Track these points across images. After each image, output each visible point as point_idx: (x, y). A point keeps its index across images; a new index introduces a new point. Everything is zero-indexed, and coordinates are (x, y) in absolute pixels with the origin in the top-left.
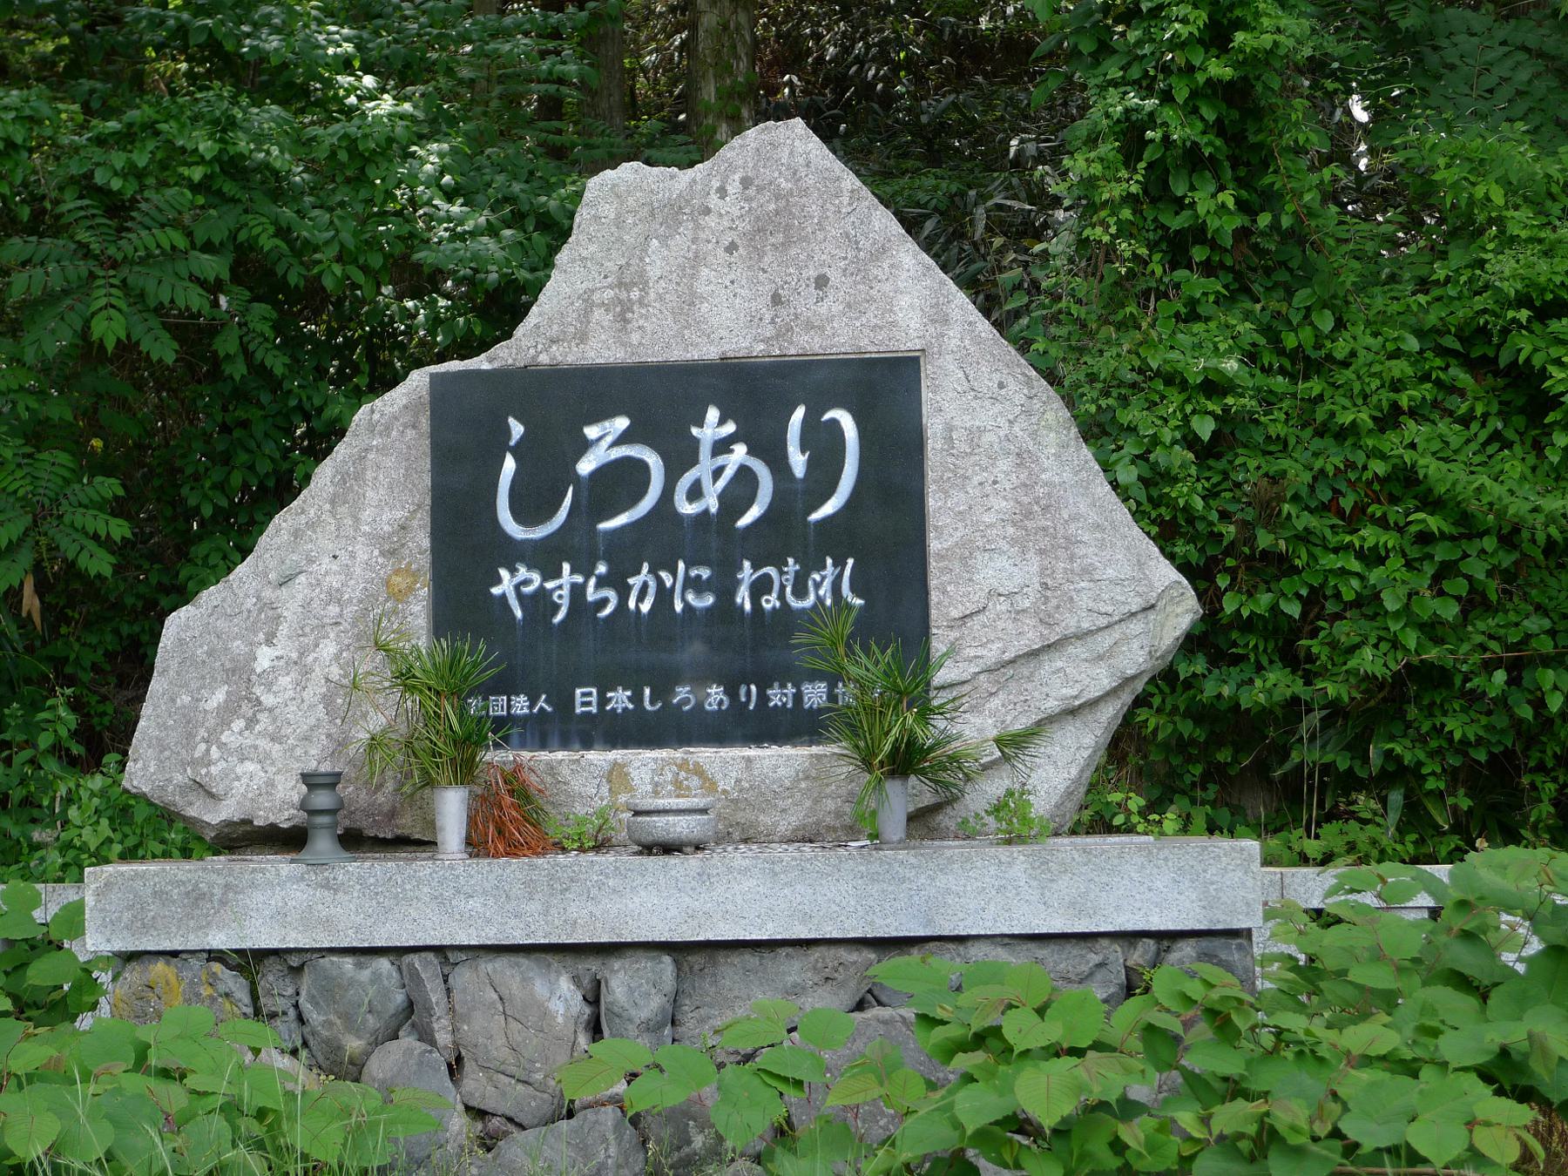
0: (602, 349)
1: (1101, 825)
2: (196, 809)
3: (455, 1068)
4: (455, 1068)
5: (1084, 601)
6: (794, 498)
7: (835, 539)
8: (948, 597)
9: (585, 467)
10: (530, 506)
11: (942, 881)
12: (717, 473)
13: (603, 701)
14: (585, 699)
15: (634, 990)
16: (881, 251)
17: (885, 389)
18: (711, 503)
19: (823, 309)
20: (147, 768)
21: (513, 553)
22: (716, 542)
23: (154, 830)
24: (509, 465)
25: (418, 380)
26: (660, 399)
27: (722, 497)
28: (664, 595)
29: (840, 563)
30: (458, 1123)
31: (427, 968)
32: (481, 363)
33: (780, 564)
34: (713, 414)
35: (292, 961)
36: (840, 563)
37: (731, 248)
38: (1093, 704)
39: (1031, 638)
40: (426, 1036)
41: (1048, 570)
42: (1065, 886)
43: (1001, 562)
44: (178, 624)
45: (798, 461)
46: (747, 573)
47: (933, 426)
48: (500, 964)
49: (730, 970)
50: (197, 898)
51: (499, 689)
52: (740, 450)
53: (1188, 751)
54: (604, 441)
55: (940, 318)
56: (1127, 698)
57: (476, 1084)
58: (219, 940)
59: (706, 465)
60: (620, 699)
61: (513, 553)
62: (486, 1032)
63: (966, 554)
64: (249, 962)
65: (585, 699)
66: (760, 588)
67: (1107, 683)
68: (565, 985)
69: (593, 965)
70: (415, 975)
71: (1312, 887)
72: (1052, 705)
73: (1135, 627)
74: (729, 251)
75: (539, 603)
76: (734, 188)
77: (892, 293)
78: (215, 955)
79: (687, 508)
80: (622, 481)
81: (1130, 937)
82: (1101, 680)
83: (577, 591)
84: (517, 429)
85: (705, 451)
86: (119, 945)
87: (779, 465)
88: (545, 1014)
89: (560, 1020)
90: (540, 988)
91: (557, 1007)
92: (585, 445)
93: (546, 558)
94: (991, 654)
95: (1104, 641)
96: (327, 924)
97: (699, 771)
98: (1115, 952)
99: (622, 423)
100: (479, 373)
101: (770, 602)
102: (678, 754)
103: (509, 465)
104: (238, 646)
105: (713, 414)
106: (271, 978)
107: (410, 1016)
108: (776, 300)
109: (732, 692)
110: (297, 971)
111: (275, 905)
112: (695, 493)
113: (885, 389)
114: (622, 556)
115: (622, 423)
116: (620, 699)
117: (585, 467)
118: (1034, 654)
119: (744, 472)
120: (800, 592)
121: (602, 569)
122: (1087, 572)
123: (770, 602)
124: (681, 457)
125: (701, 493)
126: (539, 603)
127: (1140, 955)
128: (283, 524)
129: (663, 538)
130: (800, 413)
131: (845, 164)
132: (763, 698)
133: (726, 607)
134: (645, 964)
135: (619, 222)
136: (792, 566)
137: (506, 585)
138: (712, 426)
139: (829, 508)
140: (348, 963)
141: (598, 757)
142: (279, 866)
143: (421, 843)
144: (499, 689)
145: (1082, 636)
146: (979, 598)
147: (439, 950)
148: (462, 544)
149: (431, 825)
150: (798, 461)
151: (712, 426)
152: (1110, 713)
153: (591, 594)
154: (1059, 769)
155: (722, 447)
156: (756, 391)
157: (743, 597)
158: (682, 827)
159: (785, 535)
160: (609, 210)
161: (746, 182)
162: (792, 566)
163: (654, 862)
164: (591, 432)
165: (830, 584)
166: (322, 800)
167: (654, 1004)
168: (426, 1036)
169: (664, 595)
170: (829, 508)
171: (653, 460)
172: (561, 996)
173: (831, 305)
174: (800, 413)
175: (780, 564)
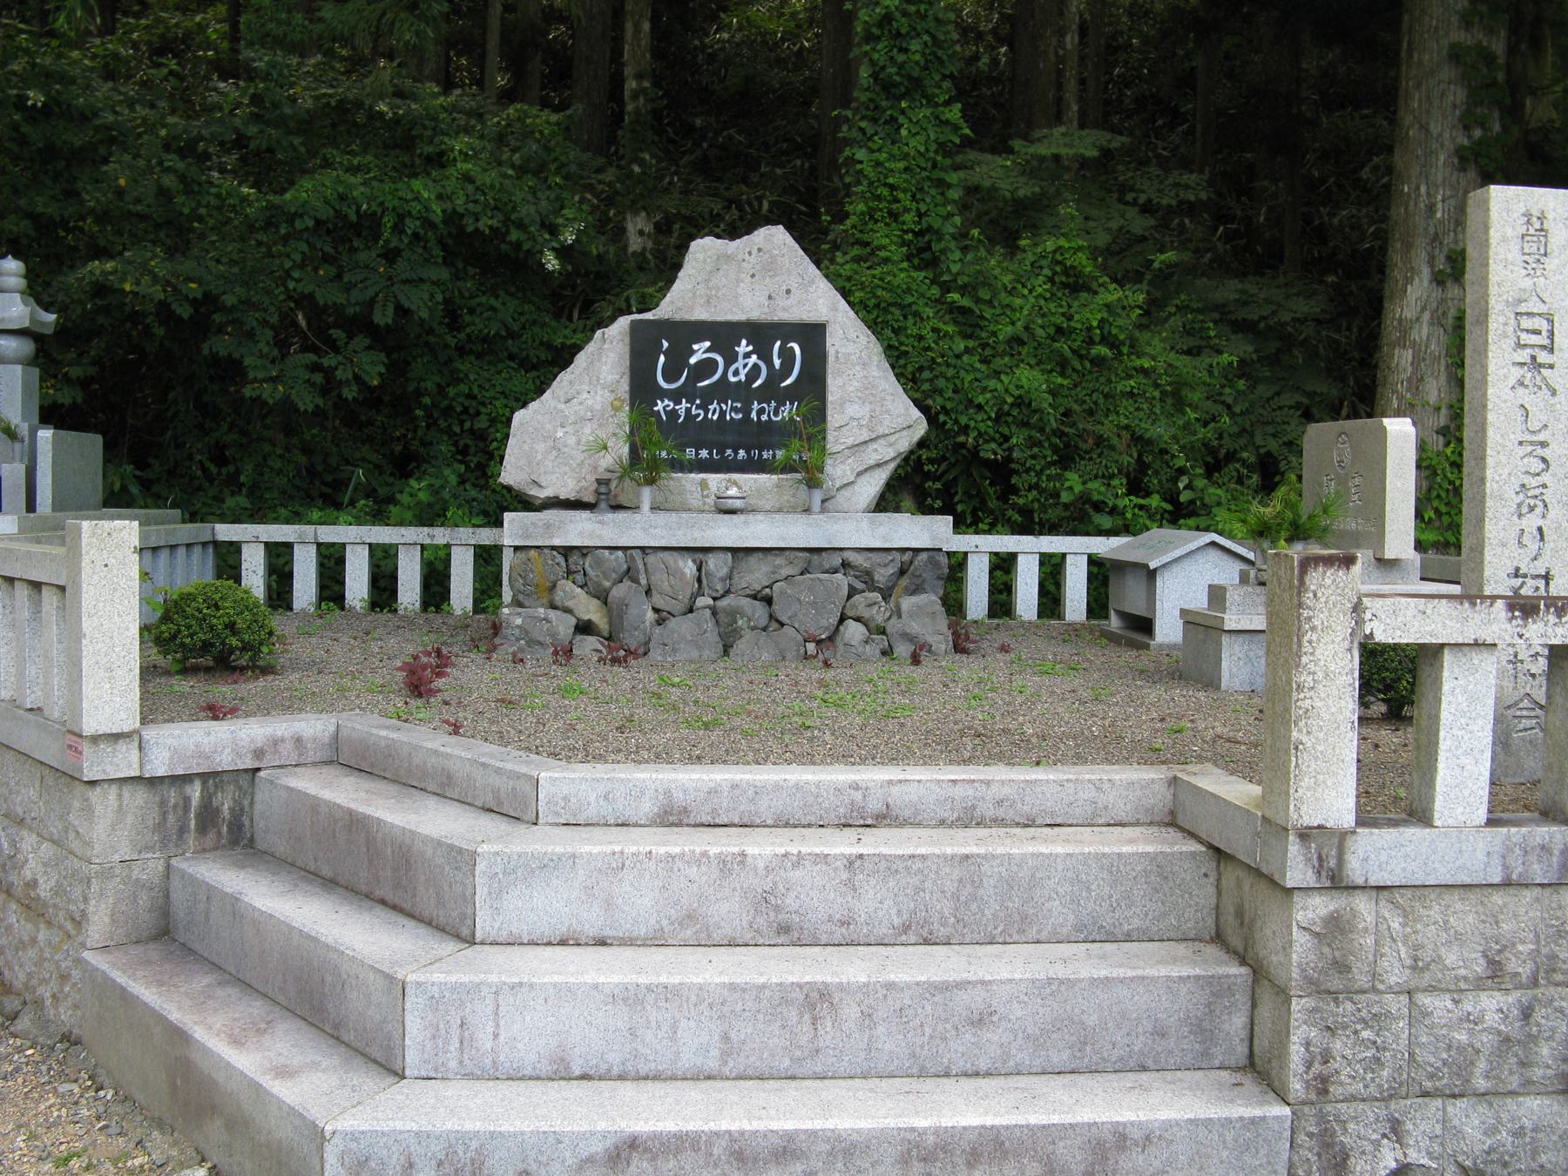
0: (701, 314)
2: (534, 492)
3: (648, 592)
4: (648, 592)
5: (886, 423)
6: (775, 377)
7: (791, 394)
8: (834, 418)
9: (693, 361)
11: (836, 527)
12: (745, 366)
13: (697, 454)
15: (717, 566)
16: (812, 282)
17: (812, 335)
19: (789, 303)
20: (511, 473)
21: (663, 394)
22: (743, 392)
23: (524, 503)
24: (662, 358)
25: (624, 322)
26: (724, 335)
28: (723, 413)
29: (792, 404)
30: (650, 616)
31: (637, 554)
32: (648, 316)
33: (769, 404)
34: (744, 342)
35: (583, 551)
36: (792, 404)
37: (753, 276)
39: (865, 436)
40: (636, 581)
41: (871, 409)
42: (882, 530)
43: (856, 406)
44: (519, 417)
45: (777, 362)
46: (756, 406)
47: (831, 351)
48: (666, 555)
49: (753, 560)
50: (548, 526)
51: (660, 445)
52: (754, 357)
53: (910, 486)
54: (700, 351)
55: (835, 309)
58: (557, 542)
59: (741, 362)
60: (704, 453)
61: (663, 394)
62: (661, 580)
64: (566, 551)
66: (761, 412)
67: (892, 455)
68: (690, 563)
69: (700, 556)
70: (632, 557)
72: (872, 462)
73: (904, 433)
75: (673, 414)
76: (755, 251)
77: (812, 296)
78: (553, 548)
79: (733, 379)
80: (707, 367)
81: (903, 550)
83: (688, 410)
84: (666, 344)
86: (517, 543)
87: (770, 364)
88: (683, 574)
90: (681, 563)
91: (687, 571)
92: (693, 352)
93: (676, 396)
94: (850, 441)
95: (892, 439)
96: (599, 537)
97: (735, 483)
98: (897, 555)
99: (708, 344)
101: (764, 418)
102: (727, 476)
103: (662, 358)
105: (744, 342)
106: (574, 558)
107: (629, 574)
108: (770, 297)
109: (748, 452)
110: (584, 555)
111: (578, 529)
112: (736, 373)
113: (812, 335)
114: (707, 396)
115: (708, 344)
116: (704, 453)
117: (693, 361)
119: (755, 366)
120: (776, 414)
122: (888, 412)
123: (764, 418)
124: (731, 358)
125: (739, 373)
126: (673, 414)
127: (907, 557)
128: (564, 377)
129: (723, 390)
130: (778, 343)
131: (1494, 743)
132: (760, 455)
134: (721, 555)
135: (705, 261)
136: (773, 404)
137: (660, 407)
138: (743, 347)
139: (788, 382)
140: (607, 552)
142: (585, 514)
143: (636, 508)
144: (660, 445)
146: (846, 419)
147: (642, 549)
148: (642, 389)
150: (777, 362)
151: (743, 347)
152: (892, 466)
153: (694, 412)
154: (873, 486)
156: (761, 334)
157: (754, 415)
158: (738, 504)
159: (771, 391)
160: (701, 256)
161: (759, 250)
164: (695, 347)
166: (603, 489)
167: (724, 571)
168: (636, 581)
169: (723, 413)
170: (788, 382)
171: (720, 359)
172: (688, 567)
173: (793, 300)
174: (778, 343)
175: (769, 404)
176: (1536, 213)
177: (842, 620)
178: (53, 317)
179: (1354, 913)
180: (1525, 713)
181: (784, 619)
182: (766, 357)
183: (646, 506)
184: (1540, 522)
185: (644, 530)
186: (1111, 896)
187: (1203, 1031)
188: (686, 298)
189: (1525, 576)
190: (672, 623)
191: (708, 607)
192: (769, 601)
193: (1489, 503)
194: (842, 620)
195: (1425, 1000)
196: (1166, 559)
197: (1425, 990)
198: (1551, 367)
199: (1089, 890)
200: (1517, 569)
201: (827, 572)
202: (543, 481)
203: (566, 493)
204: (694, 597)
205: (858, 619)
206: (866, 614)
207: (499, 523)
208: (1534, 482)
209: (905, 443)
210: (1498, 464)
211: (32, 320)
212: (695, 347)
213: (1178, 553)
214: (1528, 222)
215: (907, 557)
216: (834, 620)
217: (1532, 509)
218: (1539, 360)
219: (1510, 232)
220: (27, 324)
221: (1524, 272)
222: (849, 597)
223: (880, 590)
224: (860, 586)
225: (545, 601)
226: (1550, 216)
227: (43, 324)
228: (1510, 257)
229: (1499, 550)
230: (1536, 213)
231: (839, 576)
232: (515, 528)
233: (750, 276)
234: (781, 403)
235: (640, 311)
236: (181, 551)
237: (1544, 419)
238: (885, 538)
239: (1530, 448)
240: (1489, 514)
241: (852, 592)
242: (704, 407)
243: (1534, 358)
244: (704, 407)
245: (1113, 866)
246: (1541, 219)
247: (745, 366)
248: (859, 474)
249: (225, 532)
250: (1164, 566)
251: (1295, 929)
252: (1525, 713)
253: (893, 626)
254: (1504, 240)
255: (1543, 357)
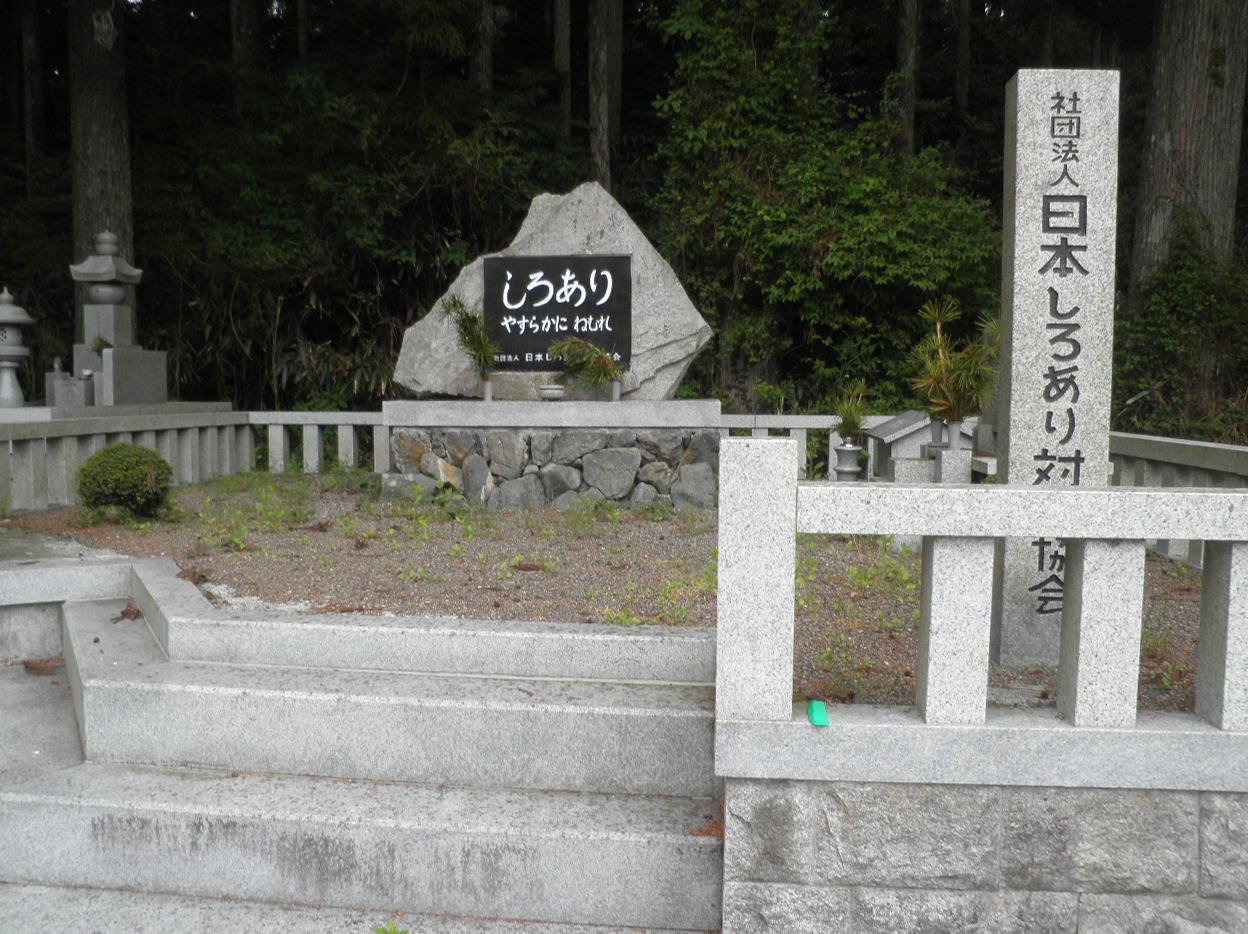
0: (536, 251)
1: (676, 397)
3: (489, 463)
4: (489, 463)
6: (593, 297)
8: (637, 328)
10: (513, 299)
12: (569, 290)
14: (528, 357)
17: (620, 265)
18: (567, 299)
20: (399, 377)
22: (568, 310)
23: (403, 393)
25: (480, 260)
26: (553, 267)
27: (571, 298)
28: (553, 326)
32: (499, 255)
33: (587, 317)
34: (568, 272)
36: (605, 317)
38: (680, 361)
39: (662, 340)
40: (480, 453)
41: (667, 317)
44: (409, 332)
45: (594, 287)
46: (578, 321)
54: (536, 280)
56: (690, 360)
57: (495, 467)
62: (498, 453)
63: (641, 318)
65: (528, 357)
66: (581, 324)
67: (684, 355)
71: (910, 140)
74: (578, 221)
75: (515, 328)
77: (628, 238)
80: (541, 291)
82: (681, 354)
83: (527, 325)
85: (566, 283)
87: (588, 288)
89: (107, 236)
92: (530, 281)
93: (517, 314)
95: (683, 343)
100: (498, 259)
101: (584, 329)
104: (427, 340)
112: (563, 295)
113: (620, 265)
116: (539, 357)
118: (661, 346)
120: (593, 325)
121: (534, 318)
123: (584, 329)
124: (558, 284)
125: (564, 294)
129: (553, 309)
130: (594, 273)
133: (571, 330)
136: (591, 318)
137: (506, 322)
138: (568, 276)
141: (532, 374)
144: (491, 346)
145: (676, 341)
149: (483, 393)
150: (594, 287)
151: (568, 276)
152: (684, 364)
153: (531, 326)
154: (669, 380)
155: (571, 282)
156: (581, 266)
157: (576, 327)
159: (591, 308)
161: (580, 201)
162: (573, 276)
163: (546, 404)
164: (532, 277)
165: (603, 323)
168: (480, 453)
169: (553, 326)
174: (594, 273)
175: (587, 317)
176: (1067, 95)
177: (637, 481)
178: (138, 272)
179: (790, 806)
180: (1052, 594)
181: (590, 482)
182: (586, 283)
183: (488, 396)
184: (1070, 405)
185: (484, 413)
186: (620, 754)
187: (673, 894)
188: (528, 241)
189: (1054, 458)
190: (506, 485)
191: (536, 473)
192: (580, 468)
193: (1015, 386)
194: (637, 481)
195: (869, 896)
196: (897, 435)
197: (868, 886)
198: (1084, 248)
199: (598, 746)
200: (1045, 451)
201: (625, 446)
202: (420, 377)
203: (437, 389)
204: (524, 465)
205: (649, 482)
206: (655, 479)
207: (379, 408)
208: (1064, 365)
209: (693, 346)
210: (1023, 348)
211: (118, 272)
212: (532, 277)
213: (907, 430)
214: (1059, 107)
215: (558, 433)
216: (629, 482)
217: (1061, 393)
218: (1069, 243)
219: (1039, 115)
220: (113, 276)
221: (1054, 155)
222: (641, 466)
223: (667, 460)
224: (649, 456)
225: (415, 468)
226: (1083, 97)
227: (134, 277)
228: (1039, 140)
229: (1025, 433)
230: (1067, 95)
231: (634, 449)
232: (392, 413)
233: (578, 220)
234: (596, 318)
235: (492, 250)
236: (211, 434)
237: (1075, 302)
238: (667, 419)
239: (1059, 332)
240: (1015, 396)
241: (644, 461)
242: (539, 322)
243: (1064, 240)
244: (539, 322)
245: (625, 729)
246: (1075, 99)
247: (569, 290)
248: (658, 371)
249: (257, 417)
250: (897, 441)
251: (728, 816)
252: (1052, 594)
253: (675, 488)
254: (1033, 122)
255: (1074, 239)
